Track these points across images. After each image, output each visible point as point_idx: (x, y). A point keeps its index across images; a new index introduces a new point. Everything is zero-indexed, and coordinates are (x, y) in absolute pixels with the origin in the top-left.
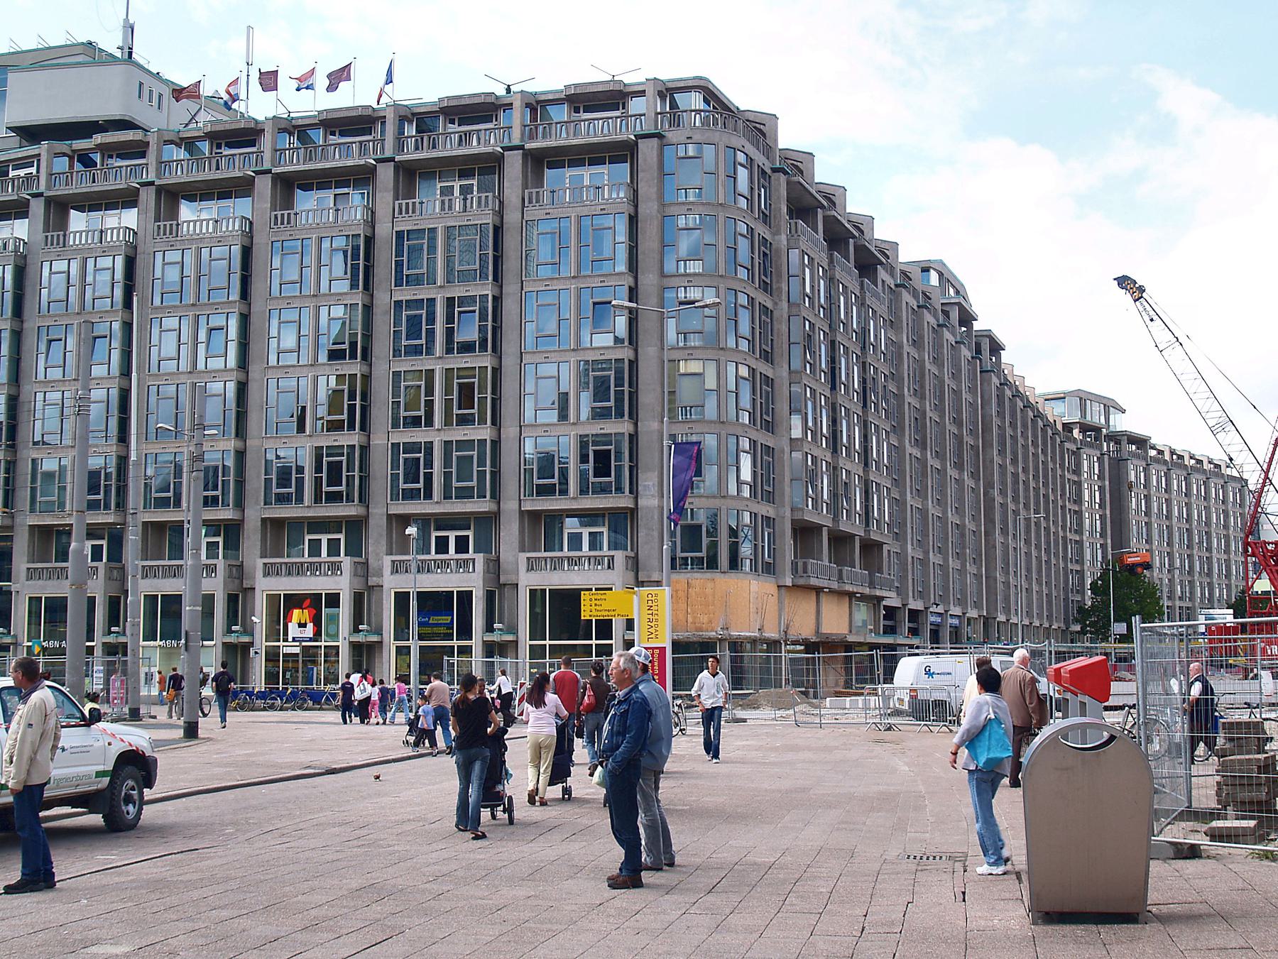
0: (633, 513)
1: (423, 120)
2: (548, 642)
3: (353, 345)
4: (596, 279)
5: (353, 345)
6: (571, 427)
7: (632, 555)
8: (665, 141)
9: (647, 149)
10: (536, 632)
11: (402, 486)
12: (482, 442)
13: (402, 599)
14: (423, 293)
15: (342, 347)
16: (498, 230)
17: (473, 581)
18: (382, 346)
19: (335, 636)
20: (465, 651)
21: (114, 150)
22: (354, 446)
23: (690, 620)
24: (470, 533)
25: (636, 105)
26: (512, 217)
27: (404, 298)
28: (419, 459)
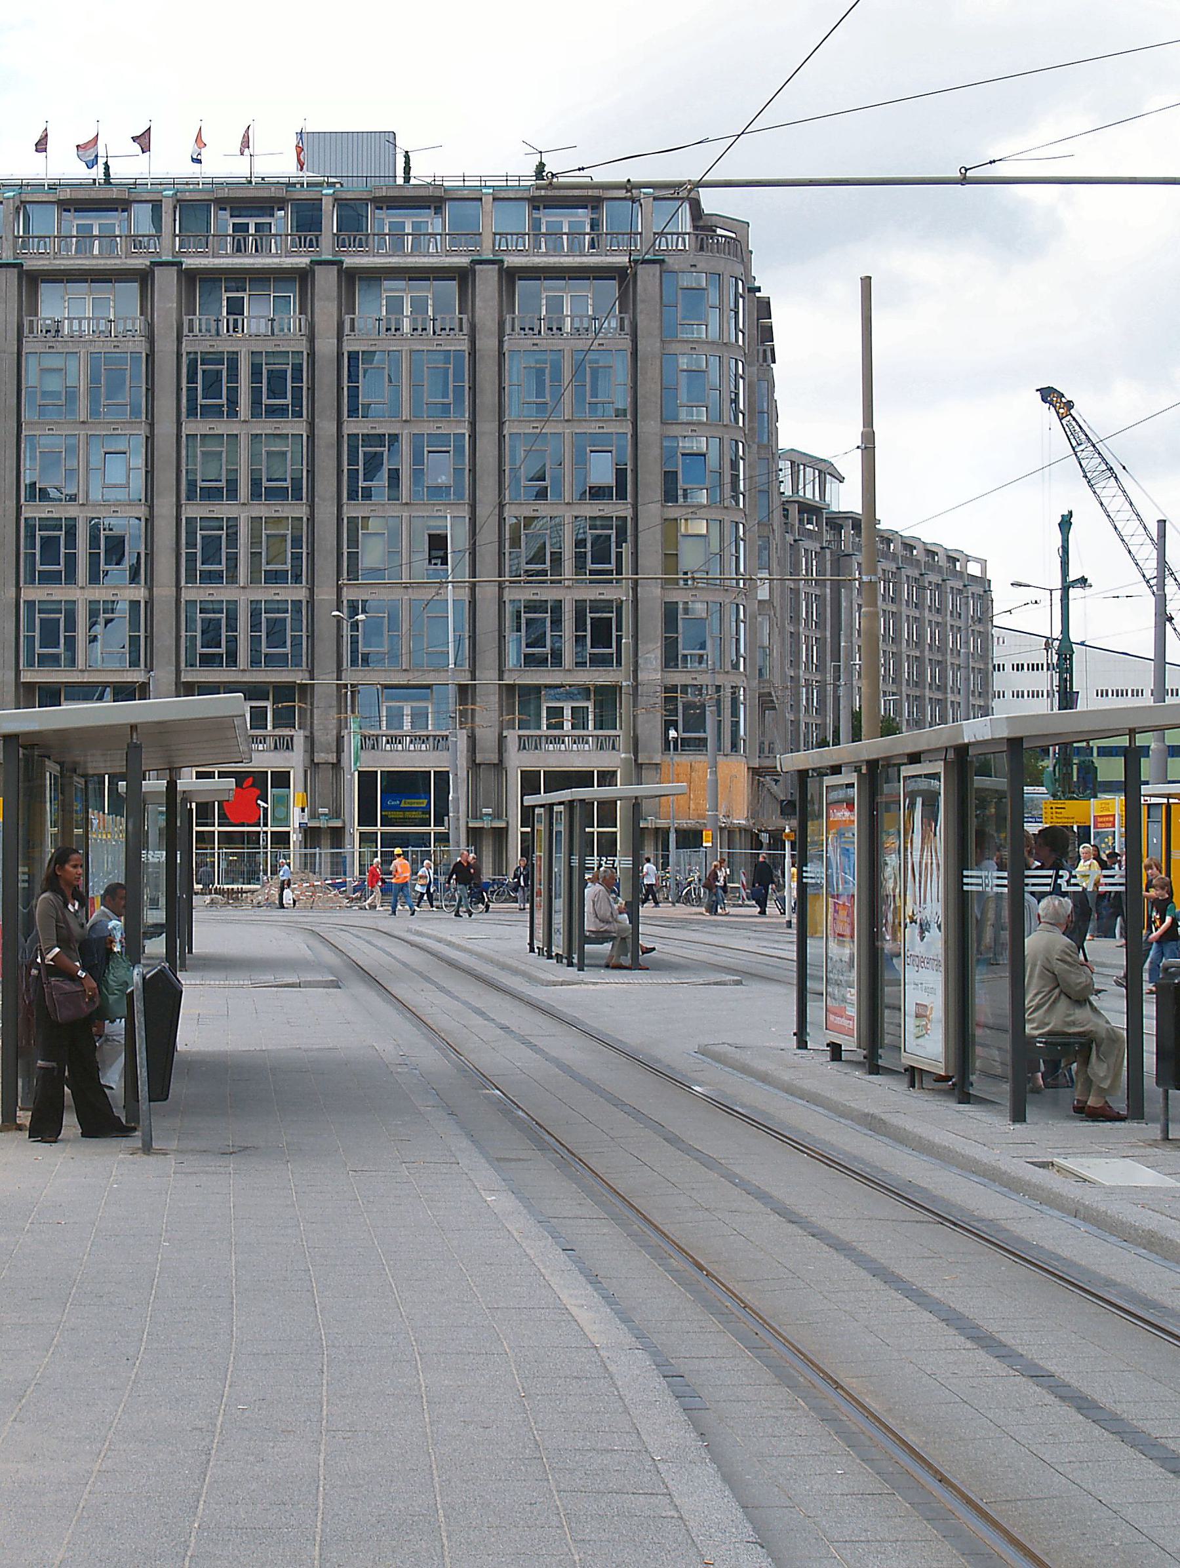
0: (305, 691)
1: (196, 206)
2: (216, 829)
3: (296, 482)
4: (593, 425)
5: (296, 482)
6: (565, 591)
7: (308, 734)
8: (665, 267)
9: (647, 277)
10: (366, 817)
11: (38, 650)
12: (297, 604)
13: (367, 779)
14: (266, 426)
15: (284, 484)
16: (150, 357)
17: (451, 760)
18: (326, 486)
19: (286, 821)
20: (443, 839)
21: (71, 204)
22: (300, 601)
23: (692, 806)
24: (269, 704)
25: (141, 216)
26: (487, 344)
27: (360, 432)
28: (611, 619)
